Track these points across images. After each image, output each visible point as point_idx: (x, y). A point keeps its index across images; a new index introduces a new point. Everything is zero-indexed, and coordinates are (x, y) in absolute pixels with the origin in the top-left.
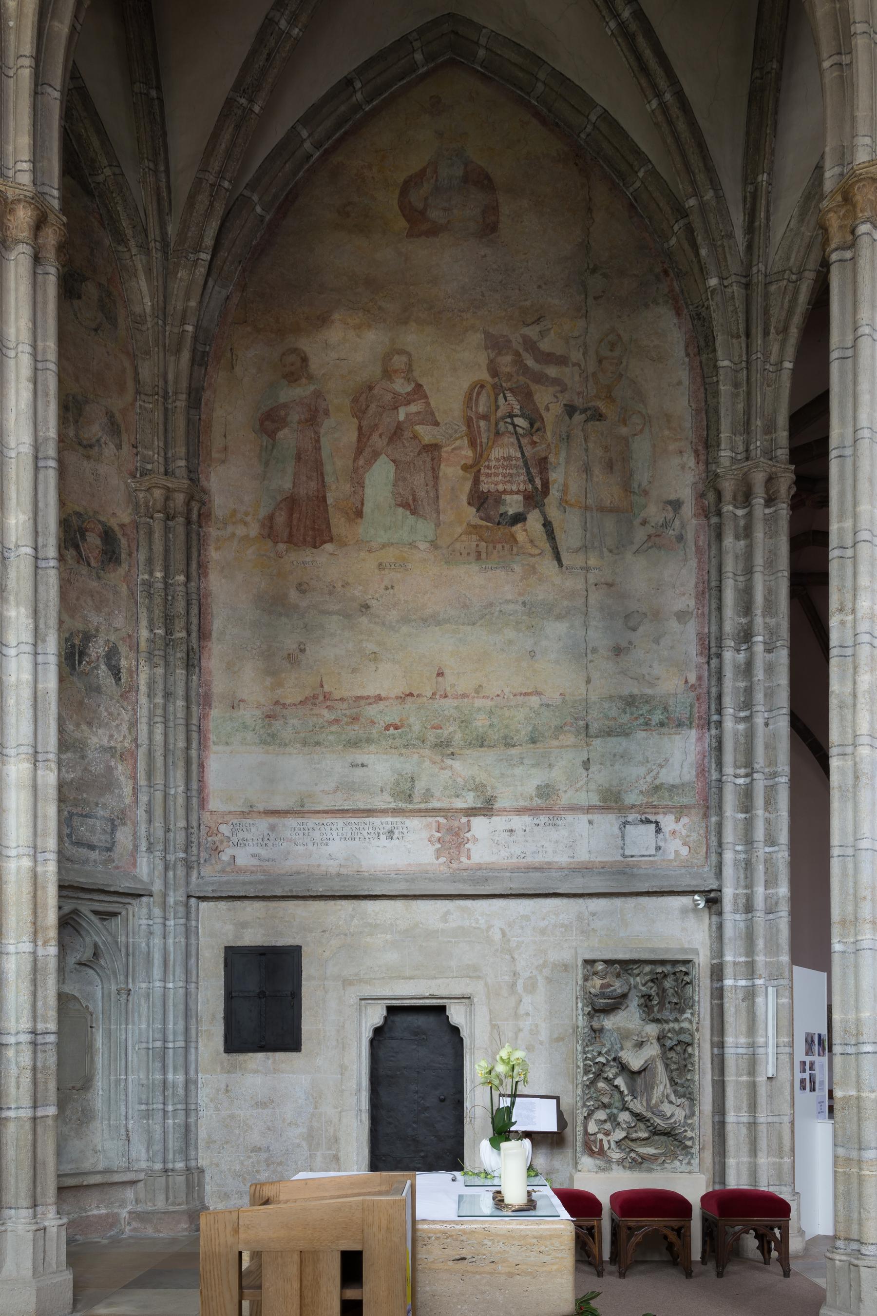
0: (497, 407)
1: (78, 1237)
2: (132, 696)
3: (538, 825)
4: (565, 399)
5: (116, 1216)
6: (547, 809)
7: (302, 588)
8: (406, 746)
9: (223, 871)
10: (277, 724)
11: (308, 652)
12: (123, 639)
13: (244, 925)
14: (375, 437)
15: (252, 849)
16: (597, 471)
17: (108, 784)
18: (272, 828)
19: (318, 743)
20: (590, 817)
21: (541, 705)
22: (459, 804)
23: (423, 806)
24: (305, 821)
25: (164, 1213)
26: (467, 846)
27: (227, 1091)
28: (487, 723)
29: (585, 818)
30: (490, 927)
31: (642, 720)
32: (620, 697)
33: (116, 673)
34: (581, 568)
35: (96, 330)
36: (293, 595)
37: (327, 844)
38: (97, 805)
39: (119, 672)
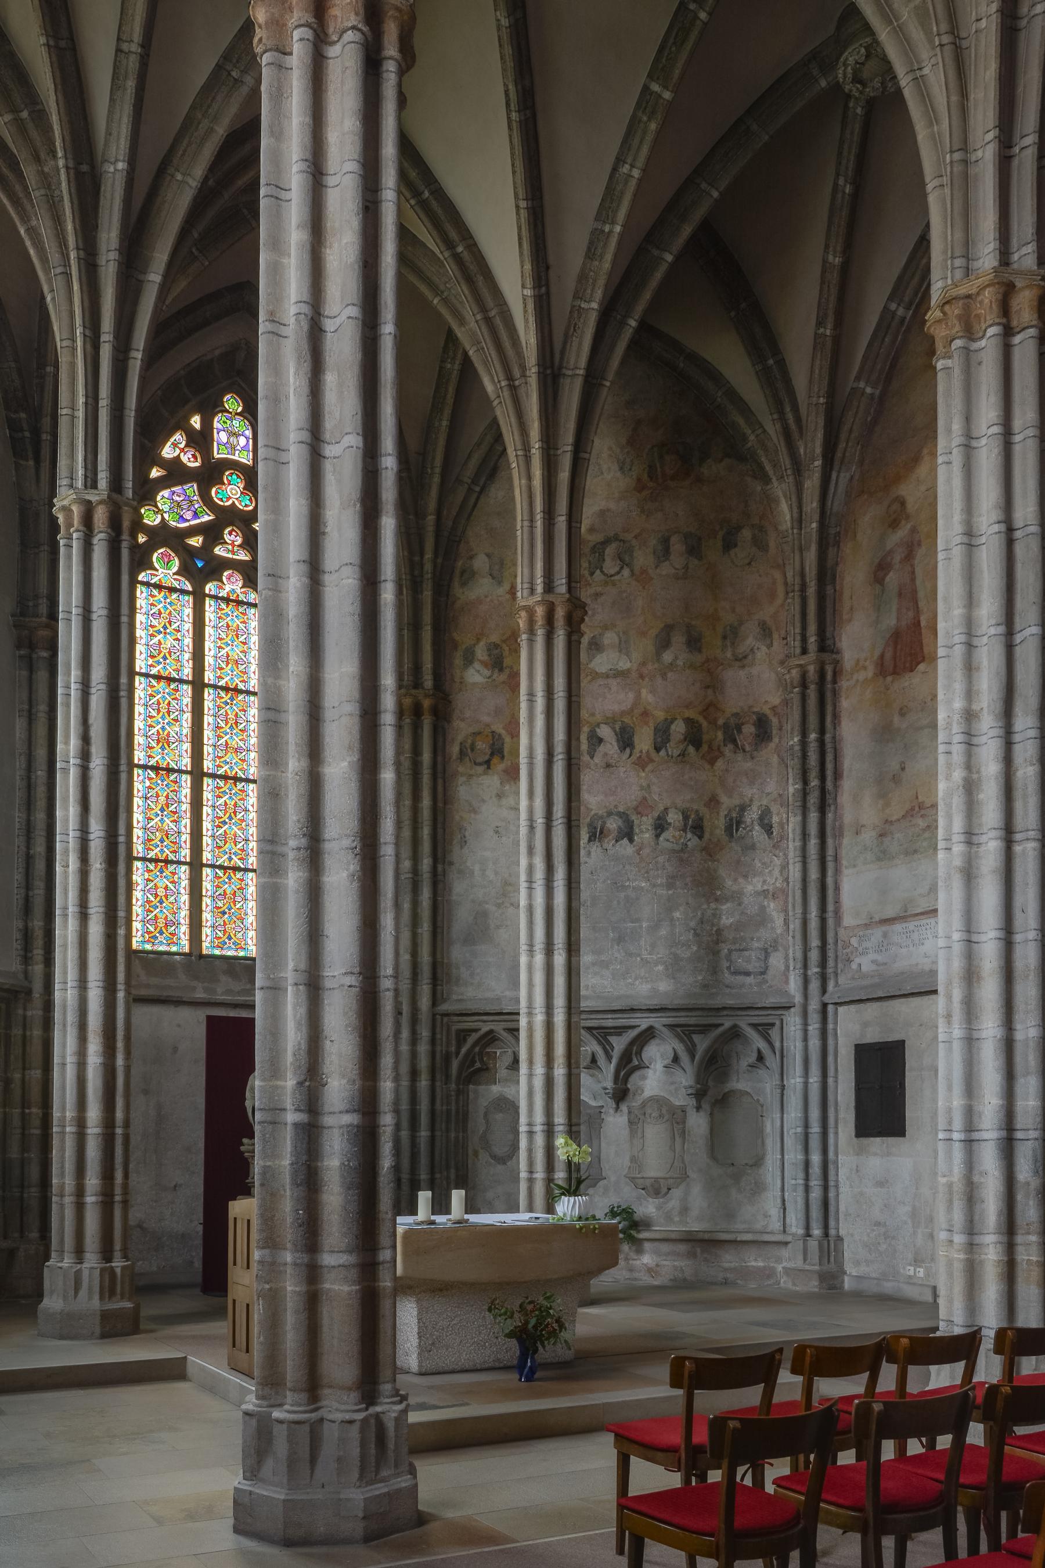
1: (739, 1282)
2: (783, 844)
7: (902, 713)
9: (853, 978)
10: (887, 840)
11: (907, 769)
12: (775, 800)
13: (865, 1025)
15: (872, 956)
17: (762, 919)
18: (885, 935)
19: (915, 851)
24: (906, 925)
25: (800, 1270)
27: (857, 1171)
33: (768, 829)
35: (749, 564)
36: (896, 719)
37: (923, 944)
38: (752, 939)
39: (771, 827)
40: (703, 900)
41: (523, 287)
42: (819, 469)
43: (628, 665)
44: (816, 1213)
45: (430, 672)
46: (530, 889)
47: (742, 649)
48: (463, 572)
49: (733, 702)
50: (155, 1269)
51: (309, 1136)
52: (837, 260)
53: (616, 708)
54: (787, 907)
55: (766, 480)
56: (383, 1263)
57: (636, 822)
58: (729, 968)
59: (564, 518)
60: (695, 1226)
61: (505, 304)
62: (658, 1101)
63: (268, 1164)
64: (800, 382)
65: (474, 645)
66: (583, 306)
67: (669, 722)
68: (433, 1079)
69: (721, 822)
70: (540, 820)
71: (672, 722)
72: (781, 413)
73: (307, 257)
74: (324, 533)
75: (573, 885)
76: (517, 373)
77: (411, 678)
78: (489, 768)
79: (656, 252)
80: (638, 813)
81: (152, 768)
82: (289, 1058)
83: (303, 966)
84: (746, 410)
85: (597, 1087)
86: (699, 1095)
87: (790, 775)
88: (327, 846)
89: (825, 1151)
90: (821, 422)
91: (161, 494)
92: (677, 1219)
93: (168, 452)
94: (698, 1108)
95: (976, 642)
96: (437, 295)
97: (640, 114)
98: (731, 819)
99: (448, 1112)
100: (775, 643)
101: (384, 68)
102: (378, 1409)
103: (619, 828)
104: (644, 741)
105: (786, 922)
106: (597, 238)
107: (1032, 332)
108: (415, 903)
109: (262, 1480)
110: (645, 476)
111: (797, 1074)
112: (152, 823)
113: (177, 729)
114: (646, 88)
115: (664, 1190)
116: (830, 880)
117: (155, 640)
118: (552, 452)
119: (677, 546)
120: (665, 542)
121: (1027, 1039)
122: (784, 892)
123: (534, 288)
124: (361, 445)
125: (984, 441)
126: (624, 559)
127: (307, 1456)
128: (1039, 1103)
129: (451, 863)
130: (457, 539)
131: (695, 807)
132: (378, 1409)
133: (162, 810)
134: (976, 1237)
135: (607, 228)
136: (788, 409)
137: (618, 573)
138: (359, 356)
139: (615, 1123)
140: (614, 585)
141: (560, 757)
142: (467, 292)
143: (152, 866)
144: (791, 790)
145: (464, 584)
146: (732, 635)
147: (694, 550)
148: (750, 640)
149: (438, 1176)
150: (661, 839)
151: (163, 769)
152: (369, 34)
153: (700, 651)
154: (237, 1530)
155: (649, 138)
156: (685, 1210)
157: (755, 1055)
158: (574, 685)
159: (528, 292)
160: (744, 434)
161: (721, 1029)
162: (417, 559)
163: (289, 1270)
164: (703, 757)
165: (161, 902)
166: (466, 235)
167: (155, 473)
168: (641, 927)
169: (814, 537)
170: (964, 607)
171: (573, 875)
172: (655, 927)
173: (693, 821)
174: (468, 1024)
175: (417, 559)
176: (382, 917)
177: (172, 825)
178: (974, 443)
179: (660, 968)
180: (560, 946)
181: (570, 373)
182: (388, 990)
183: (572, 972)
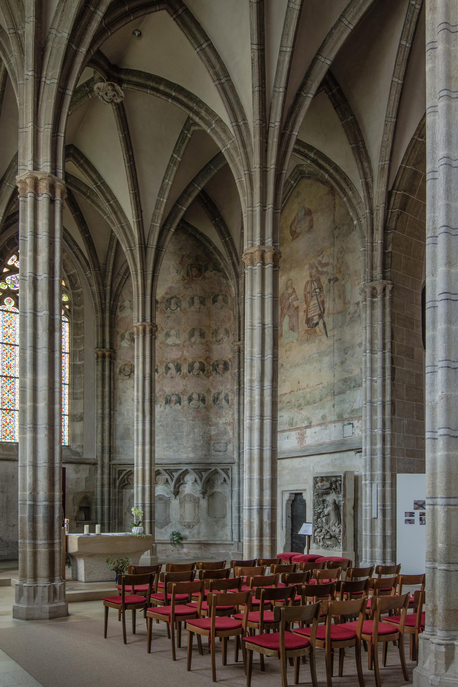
0: (312, 288)
5: (228, 553)
6: (324, 423)
8: (291, 408)
12: (230, 391)
14: (285, 310)
16: (337, 300)
17: (225, 432)
20: (334, 424)
22: (304, 425)
23: (295, 427)
29: (333, 425)
30: (310, 466)
31: (348, 387)
32: (343, 380)
33: (228, 401)
41: (133, 218)
43: (179, 342)
46: (137, 423)
48: (120, 307)
49: (216, 356)
50: (6, 554)
53: (175, 357)
55: (228, 279)
57: (182, 398)
58: (214, 449)
59: (149, 296)
60: (202, 539)
61: (128, 221)
62: (189, 495)
67: (193, 363)
68: (109, 487)
69: (211, 398)
70: (140, 400)
72: (231, 257)
73: (32, 260)
75: (153, 422)
76: (133, 245)
77: (101, 345)
78: (130, 377)
79: (180, 206)
80: (183, 394)
81: (5, 376)
82: (28, 486)
83: (31, 461)
84: (220, 254)
85: (168, 490)
86: (204, 493)
88: (39, 426)
91: (7, 278)
92: (196, 536)
93: (10, 263)
94: (204, 498)
95: (254, 358)
97: (171, 164)
98: (215, 397)
99: (115, 499)
100: (230, 336)
102: (54, 583)
104: (185, 369)
106: (158, 203)
107: (270, 265)
108: (103, 425)
109: (20, 603)
110: (185, 276)
112: (4, 396)
113: (14, 362)
114: (172, 156)
115: (192, 526)
117: (5, 331)
118: (145, 273)
119: (197, 301)
120: (192, 299)
122: (233, 423)
124: (48, 313)
125: (256, 298)
126: (178, 304)
127: (33, 596)
129: (116, 411)
132: (54, 583)
133: (8, 391)
135: (162, 199)
136: (234, 255)
137: (176, 309)
138: (48, 288)
139: (175, 503)
140: (174, 313)
141: (148, 378)
142: (114, 217)
143: (4, 412)
144: (235, 387)
145: (121, 311)
146: (215, 332)
147: (202, 302)
148: (221, 335)
149: (111, 521)
151: (8, 377)
152: (51, 195)
153: (204, 338)
154: (14, 617)
155: (174, 172)
156: (199, 533)
157: (223, 479)
158: (153, 353)
159: (135, 220)
161: (211, 471)
162: (103, 302)
163: (28, 545)
164: (205, 375)
165: (8, 424)
166: (114, 198)
167: (5, 270)
168: (183, 434)
172: (188, 435)
174: (122, 468)
175: (103, 302)
176: (56, 446)
177: (12, 397)
178: (254, 298)
179: (190, 449)
183: (152, 452)
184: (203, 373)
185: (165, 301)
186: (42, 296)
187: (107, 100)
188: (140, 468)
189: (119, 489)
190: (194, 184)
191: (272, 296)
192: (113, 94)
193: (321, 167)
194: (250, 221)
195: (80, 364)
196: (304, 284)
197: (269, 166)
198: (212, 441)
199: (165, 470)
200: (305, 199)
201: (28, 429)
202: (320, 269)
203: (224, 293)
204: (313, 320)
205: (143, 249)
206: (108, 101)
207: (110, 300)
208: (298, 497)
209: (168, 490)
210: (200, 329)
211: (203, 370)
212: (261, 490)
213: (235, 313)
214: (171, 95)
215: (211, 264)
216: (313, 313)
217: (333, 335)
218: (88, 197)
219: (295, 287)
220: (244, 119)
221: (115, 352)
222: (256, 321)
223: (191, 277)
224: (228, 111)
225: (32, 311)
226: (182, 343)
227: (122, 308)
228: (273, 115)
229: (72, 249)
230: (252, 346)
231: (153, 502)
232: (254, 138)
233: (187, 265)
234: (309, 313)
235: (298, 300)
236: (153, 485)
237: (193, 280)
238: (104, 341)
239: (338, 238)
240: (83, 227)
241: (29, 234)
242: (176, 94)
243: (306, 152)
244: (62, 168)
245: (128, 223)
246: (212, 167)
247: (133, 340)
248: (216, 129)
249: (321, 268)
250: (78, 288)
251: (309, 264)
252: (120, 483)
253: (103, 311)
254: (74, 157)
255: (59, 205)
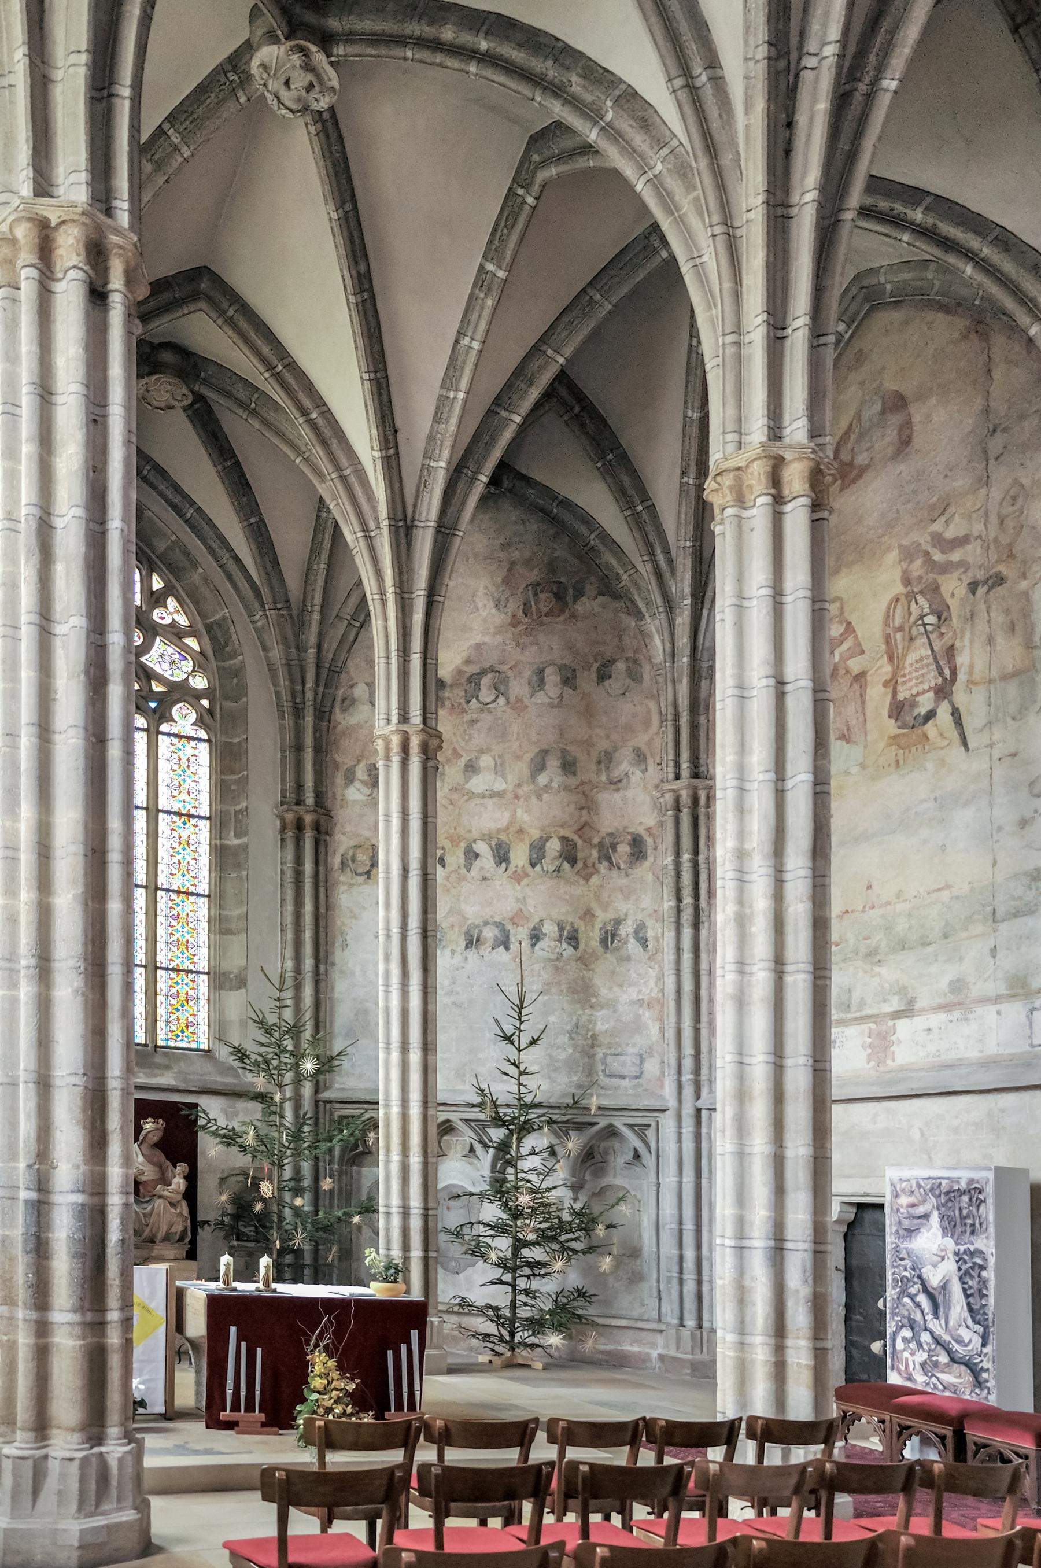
0: (910, 614)
2: (659, 957)
3: (951, 1021)
4: (967, 579)
6: (959, 1004)
8: (844, 961)
12: (650, 916)
16: (1000, 640)
17: (637, 1026)
20: (998, 1007)
21: (952, 898)
22: (888, 1009)
23: (858, 1015)
26: (892, 1049)
28: (907, 926)
29: (993, 1009)
32: (1026, 874)
33: (644, 942)
34: (986, 746)
35: (624, 694)
39: (646, 940)
40: (578, 1006)
41: (372, 448)
42: (689, 607)
44: (690, 1304)
45: (311, 790)
46: (387, 992)
47: (617, 773)
48: (343, 700)
49: (608, 822)
51: (39, 1212)
52: (696, 416)
54: (662, 1016)
55: (639, 616)
56: (111, 1322)
58: (604, 1071)
59: (418, 655)
61: (360, 463)
63: (7, 1233)
64: (669, 524)
65: (355, 766)
66: (432, 464)
67: (544, 840)
69: (596, 934)
70: (395, 930)
71: (547, 840)
74: (54, 700)
75: (429, 990)
76: (372, 525)
77: (293, 795)
78: (369, 878)
79: (504, 414)
82: (21, 1145)
85: (476, 1175)
87: (665, 891)
89: (699, 1247)
90: (689, 562)
95: (748, 786)
96: (299, 455)
98: (606, 932)
100: (650, 768)
101: (111, 299)
103: (496, 936)
104: (520, 856)
105: (662, 1030)
107: (804, 501)
110: (521, 613)
111: (671, 1174)
114: (481, 268)
116: (703, 993)
118: (406, 596)
119: (552, 677)
120: (540, 672)
121: (797, 1157)
123: (381, 450)
125: (755, 602)
126: (499, 689)
127: (30, 1488)
128: (809, 1217)
129: (333, 964)
130: (338, 669)
131: (570, 920)
132: (103, 1449)
134: (747, 1337)
135: (452, 395)
137: (494, 701)
140: (490, 712)
142: (321, 453)
145: (344, 710)
146: (606, 760)
147: (569, 680)
148: (624, 765)
150: (537, 947)
152: (90, 272)
155: (486, 314)
157: (632, 1153)
158: (430, 807)
159: (377, 454)
160: (618, 574)
161: (597, 1128)
162: (299, 687)
166: (320, 403)
169: (686, 671)
170: (736, 754)
171: (429, 981)
173: (568, 933)
178: (746, 603)
180: (415, 1045)
181: (422, 524)
182: (115, 1089)
183: (427, 1070)
184: (572, 866)
185: (463, 680)
186: (68, 573)
187: (288, 103)
188: (395, 1110)
189: (340, 1164)
190: (544, 348)
191: (808, 594)
192: (306, 83)
193: (948, 244)
194: (731, 377)
195: (239, 846)
196: (884, 606)
197: (795, 199)
198: (598, 1050)
199: (467, 1121)
200: (884, 368)
201: (23, 972)
202: (937, 556)
203: (630, 654)
204: (913, 704)
205: (402, 531)
206: (294, 107)
207: (317, 685)
208: (869, 1216)
209: (476, 1175)
210: (564, 753)
211: (572, 860)
212: (779, 1190)
213: (663, 705)
214: (476, 51)
215: (593, 579)
216: (917, 685)
217: (989, 742)
218: (254, 413)
219: (853, 619)
220: (713, 63)
221: (328, 814)
222: (755, 673)
223: (535, 617)
224: (661, 42)
225: (35, 618)
226: (511, 788)
227: (347, 703)
228: (815, 27)
229: (216, 559)
230: (742, 747)
231: (431, 1205)
232: (746, 113)
233: (524, 586)
234: (899, 688)
235: (863, 652)
236: (431, 1160)
237: (542, 624)
238: (299, 787)
239: (1001, 459)
240: (244, 499)
241: (24, 390)
242: (492, 45)
243: (899, 208)
244: (126, 196)
245: (359, 467)
246: (598, 297)
247: (375, 784)
248: (617, 124)
249: (943, 552)
250: (234, 655)
251: (900, 547)
252: (343, 1151)
253: (298, 712)
254: (210, 300)
255: (119, 306)
